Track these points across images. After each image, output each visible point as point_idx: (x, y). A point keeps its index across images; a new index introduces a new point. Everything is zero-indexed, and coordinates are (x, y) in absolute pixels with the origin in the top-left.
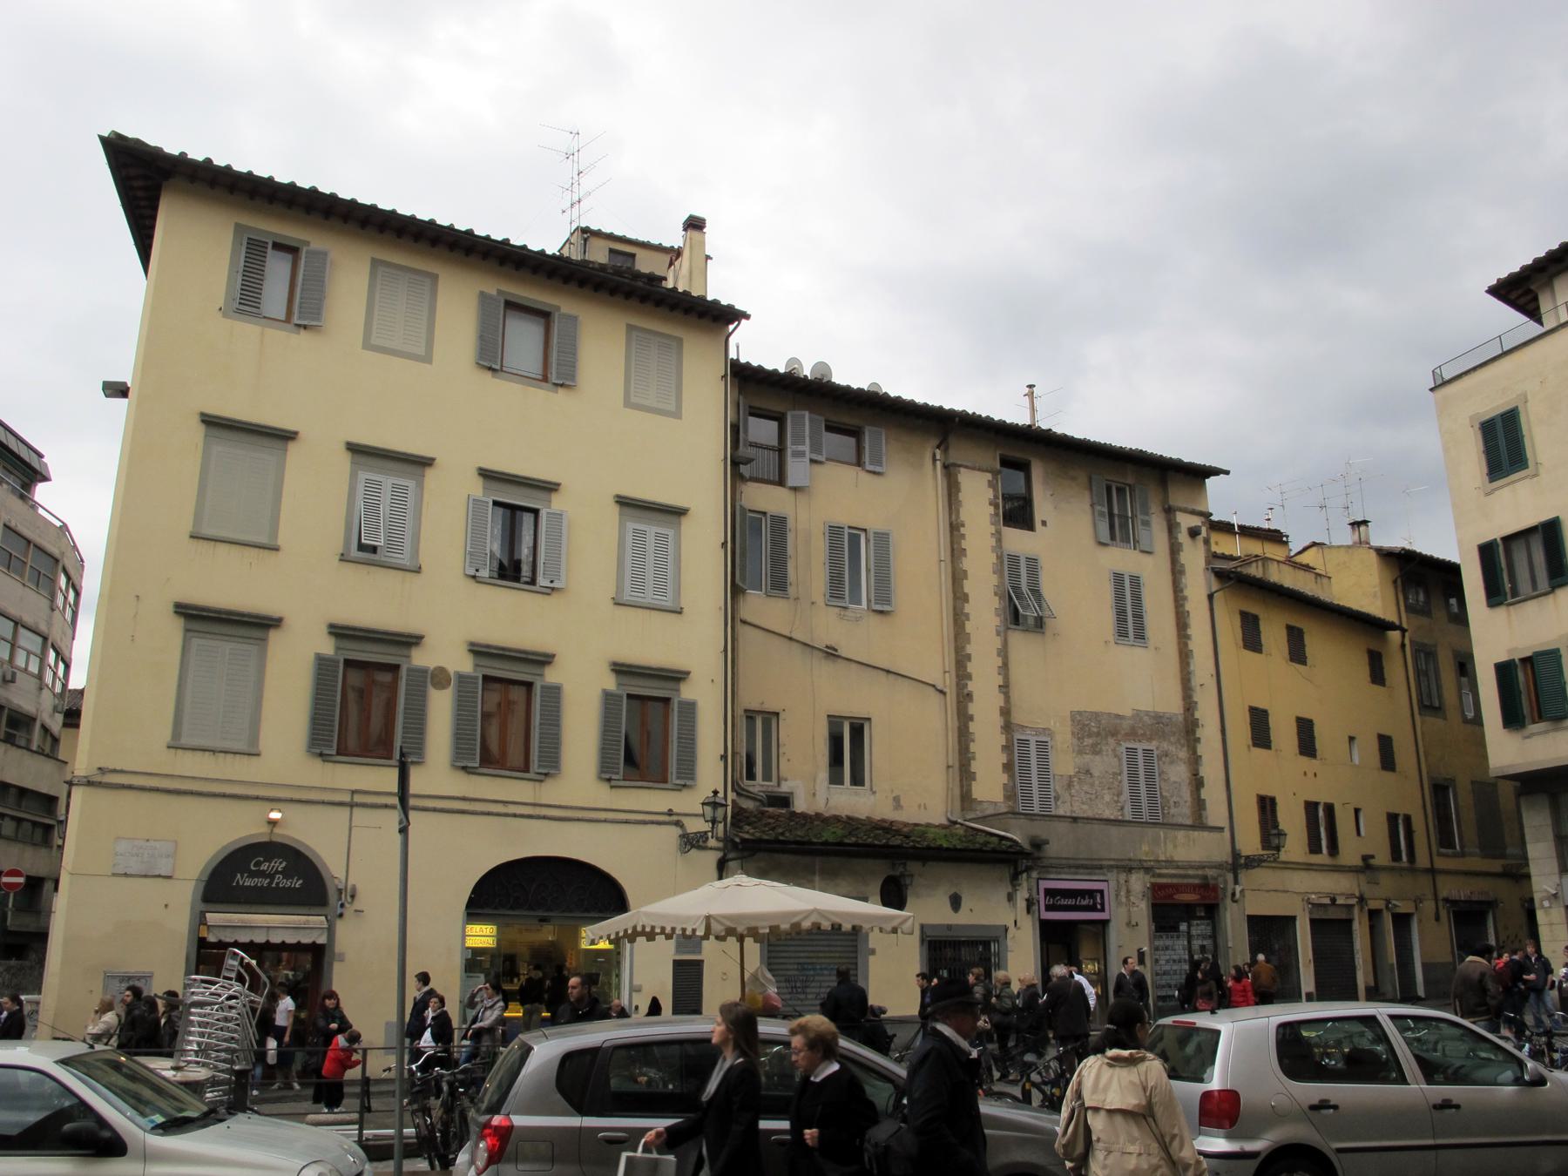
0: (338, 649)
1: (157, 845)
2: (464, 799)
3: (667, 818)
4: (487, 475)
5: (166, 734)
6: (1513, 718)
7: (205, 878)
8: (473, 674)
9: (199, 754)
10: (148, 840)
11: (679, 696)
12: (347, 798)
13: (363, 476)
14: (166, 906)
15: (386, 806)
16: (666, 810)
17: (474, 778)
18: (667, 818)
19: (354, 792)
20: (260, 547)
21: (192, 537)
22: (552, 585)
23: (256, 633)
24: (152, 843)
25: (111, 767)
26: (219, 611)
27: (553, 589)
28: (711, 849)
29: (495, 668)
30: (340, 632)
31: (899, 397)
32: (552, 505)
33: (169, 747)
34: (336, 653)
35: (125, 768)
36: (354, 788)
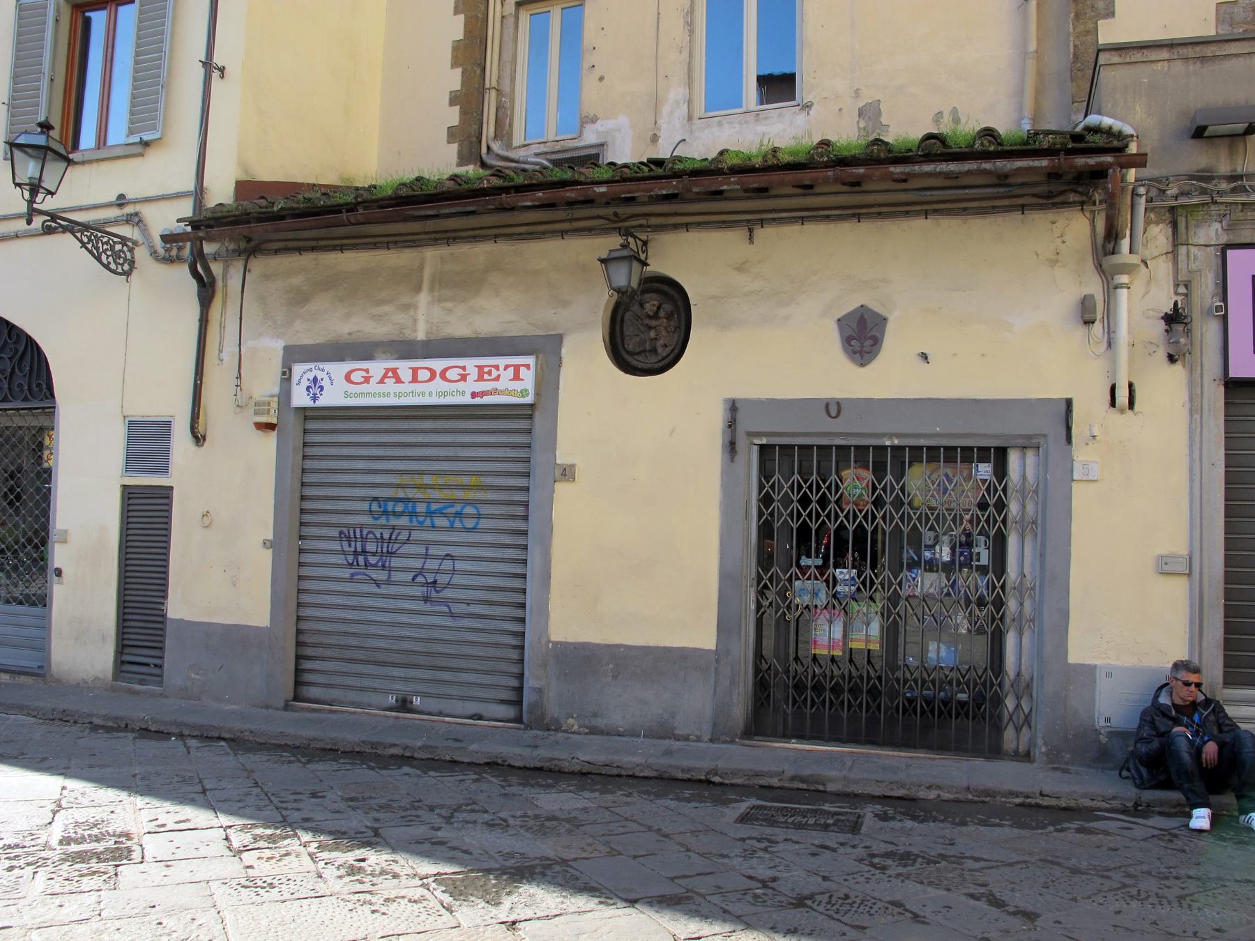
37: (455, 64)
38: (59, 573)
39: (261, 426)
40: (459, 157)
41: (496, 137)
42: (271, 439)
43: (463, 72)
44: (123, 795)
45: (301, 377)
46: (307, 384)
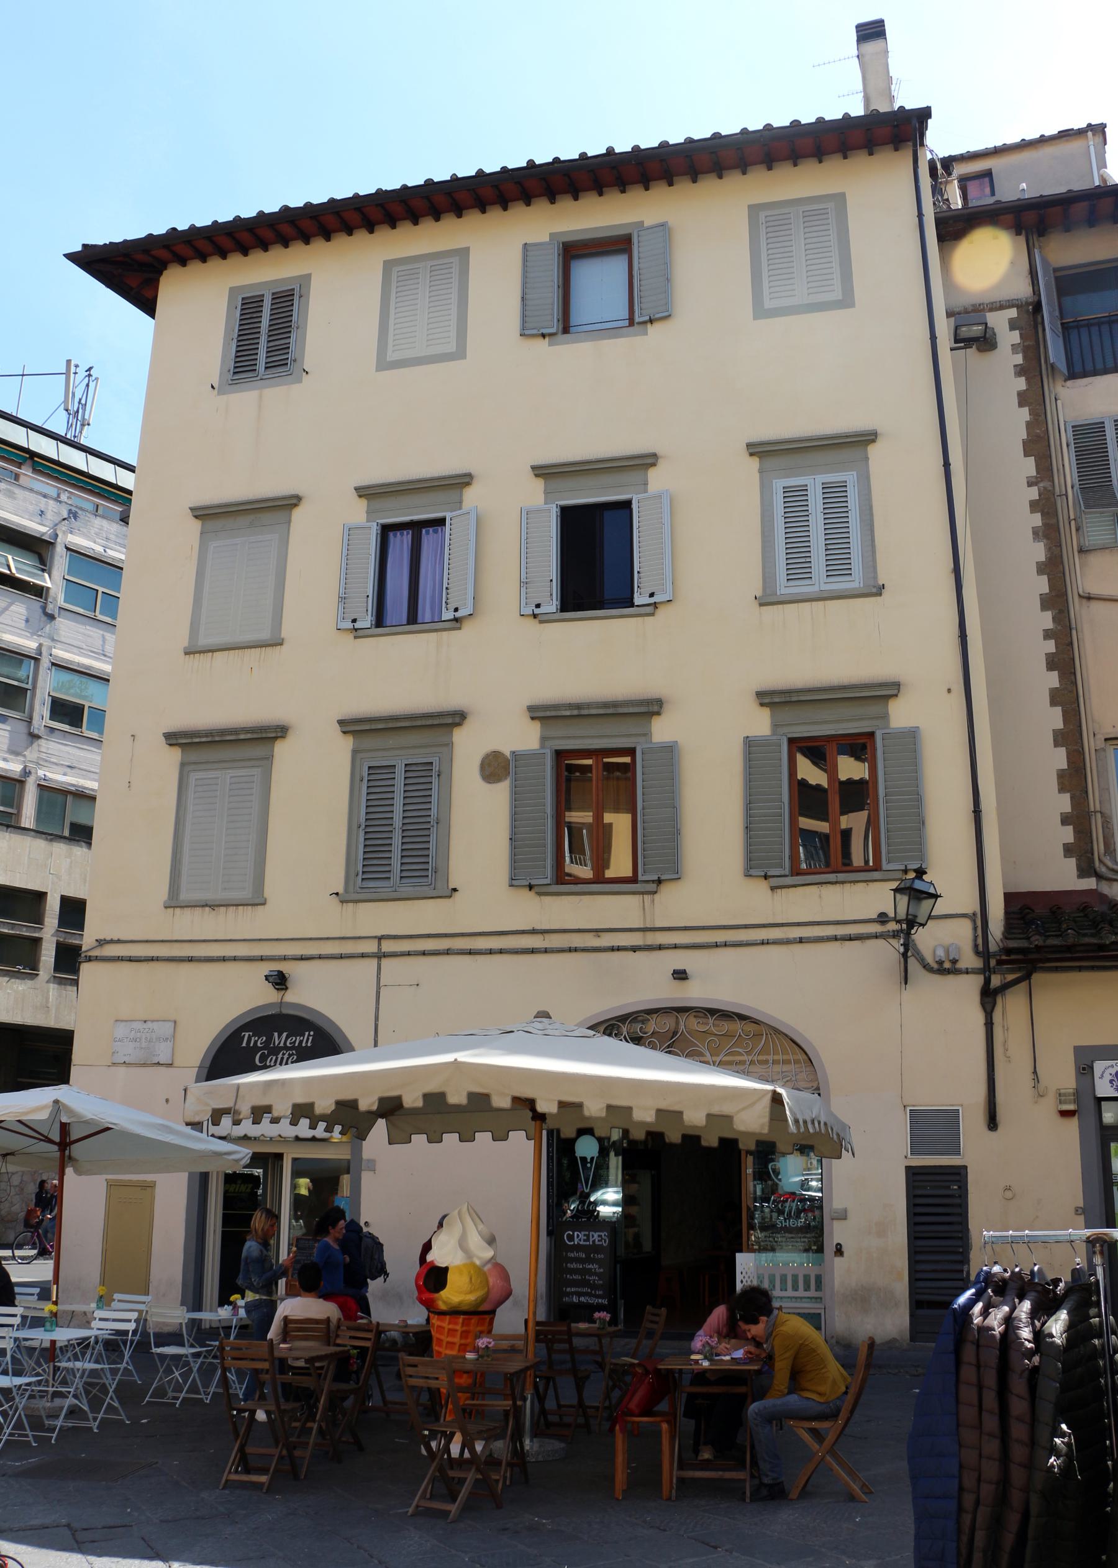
0: (775, 726)
1: (155, 1025)
2: (533, 932)
3: (876, 928)
4: (542, 472)
5: (162, 892)
6: (786, 490)
7: (208, 1064)
8: (19, 778)
9: (198, 910)
10: (145, 1022)
11: (887, 726)
12: (371, 947)
13: (779, 485)
14: (167, 1101)
15: (363, 956)
16: (875, 916)
17: (547, 900)
18: (876, 928)
19: (380, 938)
20: (261, 646)
21: (186, 653)
22: (652, 600)
23: (258, 751)
24: (149, 1025)
25: (108, 938)
26: (209, 733)
27: (655, 605)
28: (967, 972)
29: (574, 737)
30: (770, 699)
31: (150, 235)
32: (649, 487)
33: (166, 907)
34: (774, 733)
35: (122, 938)
36: (379, 934)
37: (1062, 790)
38: (839, 1251)
39: (1064, 1114)
40: (1078, 870)
41: (1105, 853)
42: (1073, 1124)
43: (1071, 798)
44: (120, 1559)
45: (1103, 1072)
46: (1110, 1078)
